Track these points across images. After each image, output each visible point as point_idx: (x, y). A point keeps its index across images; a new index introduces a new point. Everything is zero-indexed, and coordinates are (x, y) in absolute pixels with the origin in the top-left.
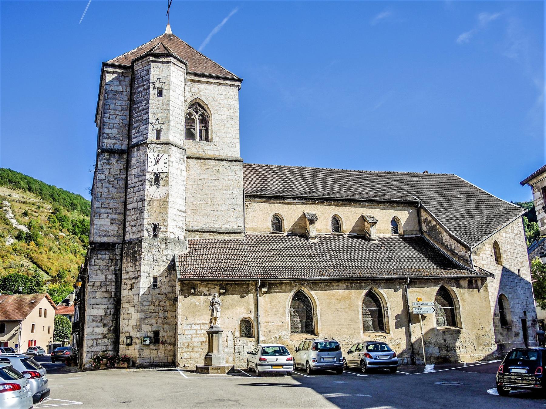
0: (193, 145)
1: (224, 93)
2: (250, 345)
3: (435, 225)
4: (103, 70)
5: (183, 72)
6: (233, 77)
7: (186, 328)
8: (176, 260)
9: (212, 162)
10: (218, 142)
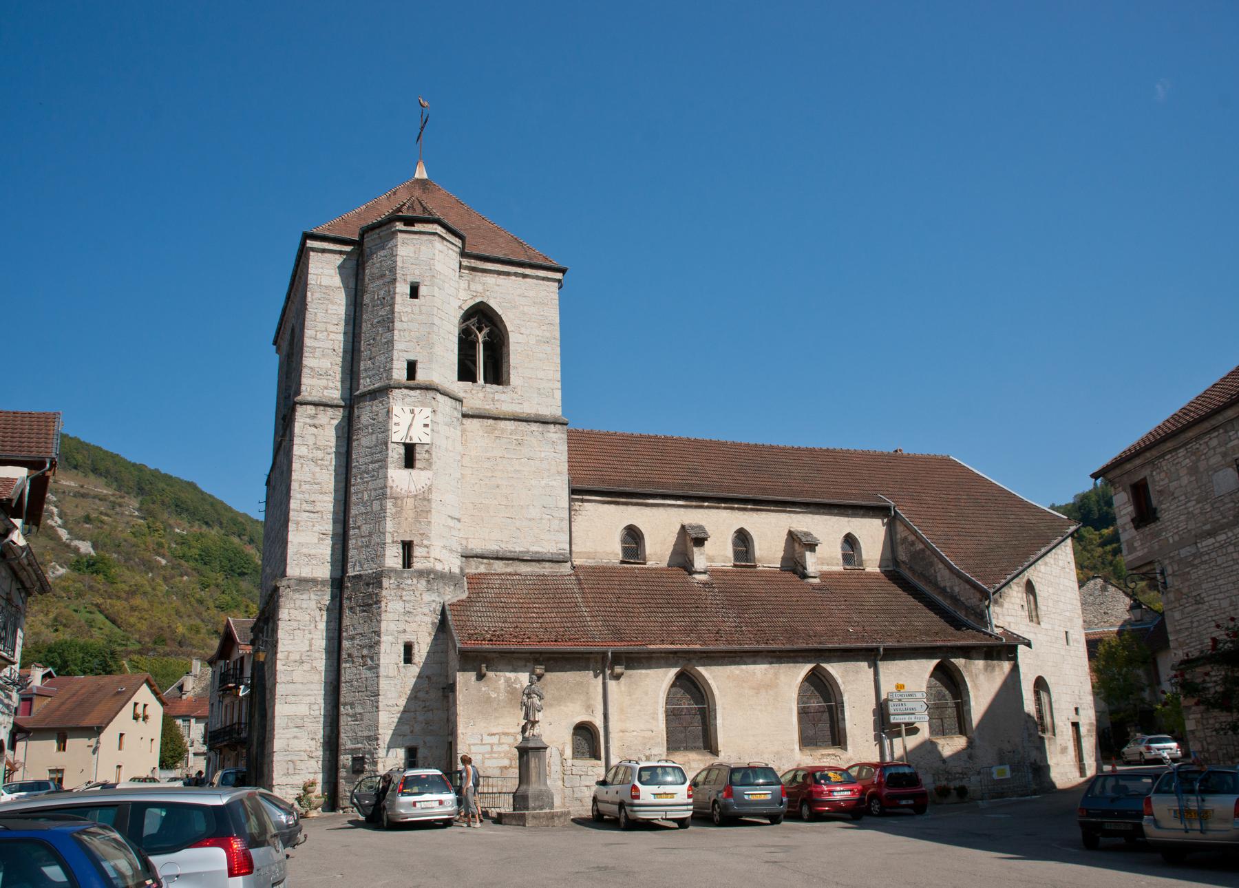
0: (474, 392)
1: (532, 294)
2: (592, 773)
3: (923, 550)
4: (303, 244)
5: (456, 252)
6: (549, 264)
7: (472, 742)
8: (448, 613)
9: (510, 425)
10: (520, 388)
